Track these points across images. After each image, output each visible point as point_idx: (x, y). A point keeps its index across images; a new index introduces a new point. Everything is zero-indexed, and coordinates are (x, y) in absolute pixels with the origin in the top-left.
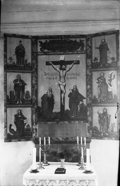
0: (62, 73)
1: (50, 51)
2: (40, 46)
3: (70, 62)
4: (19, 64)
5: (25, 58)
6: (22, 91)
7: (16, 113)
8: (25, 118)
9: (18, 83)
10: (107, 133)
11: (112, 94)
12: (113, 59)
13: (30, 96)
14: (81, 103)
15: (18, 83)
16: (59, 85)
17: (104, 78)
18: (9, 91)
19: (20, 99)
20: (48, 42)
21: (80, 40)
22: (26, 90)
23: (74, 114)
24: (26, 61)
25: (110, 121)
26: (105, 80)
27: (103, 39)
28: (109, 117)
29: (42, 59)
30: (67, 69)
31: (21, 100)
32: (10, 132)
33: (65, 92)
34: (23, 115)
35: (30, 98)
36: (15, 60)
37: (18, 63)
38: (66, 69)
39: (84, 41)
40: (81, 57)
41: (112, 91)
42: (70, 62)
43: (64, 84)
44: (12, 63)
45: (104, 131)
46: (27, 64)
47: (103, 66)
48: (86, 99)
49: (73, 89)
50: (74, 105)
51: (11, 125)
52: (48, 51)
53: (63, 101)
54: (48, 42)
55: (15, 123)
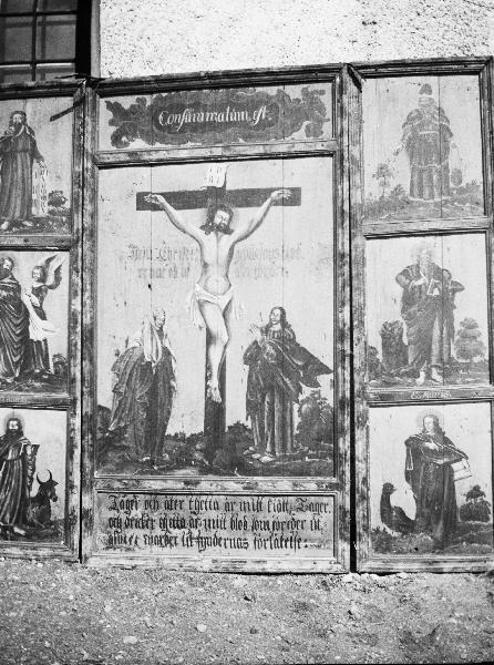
0: (216, 246)
1: (158, 145)
2: (112, 123)
3: (250, 197)
4: (421, 195)
5: (453, 162)
6: (442, 322)
7: (415, 431)
8: (461, 456)
9: (420, 282)
10: (20, 528)
11: (47, 355)
12: (55, 200)
13: (481, 344)
14: (307, 391)
15: (420, 282)
16: (201, 305)
17: (13, 278)
18: (380, 327)
19: (434, 362)
20: (148, 104)
21: (305, 92)
22: (459, 316)
23: (273, 444)
24: (458, 175)
25: (34, 470)
26: (18, 288)
27: (17, 112)
28: (29, 452)
29: (114, 185)
30: (239, 228)
31: (435, 366)
32: (384, 519)
33: (225, 338)
34: (446, 441)
35: (482, 355)
36: (402, 176)
37: (416, 191)
38: (232, 227)
39: (322, 92)
40: (313, 176)
41: (45, 340)
42: (250, 197)
43: (223, 301)
44: (388, 191)
45: (8, 516)
46: (462, 191)
47: (9, 229)
48: (331, 376)
49: (266, 322)
50: (272, 404)
51: (388, 490)
52: (149, 147)
53: (214, 383)
54: (148, 104)
55: (407, 479)
